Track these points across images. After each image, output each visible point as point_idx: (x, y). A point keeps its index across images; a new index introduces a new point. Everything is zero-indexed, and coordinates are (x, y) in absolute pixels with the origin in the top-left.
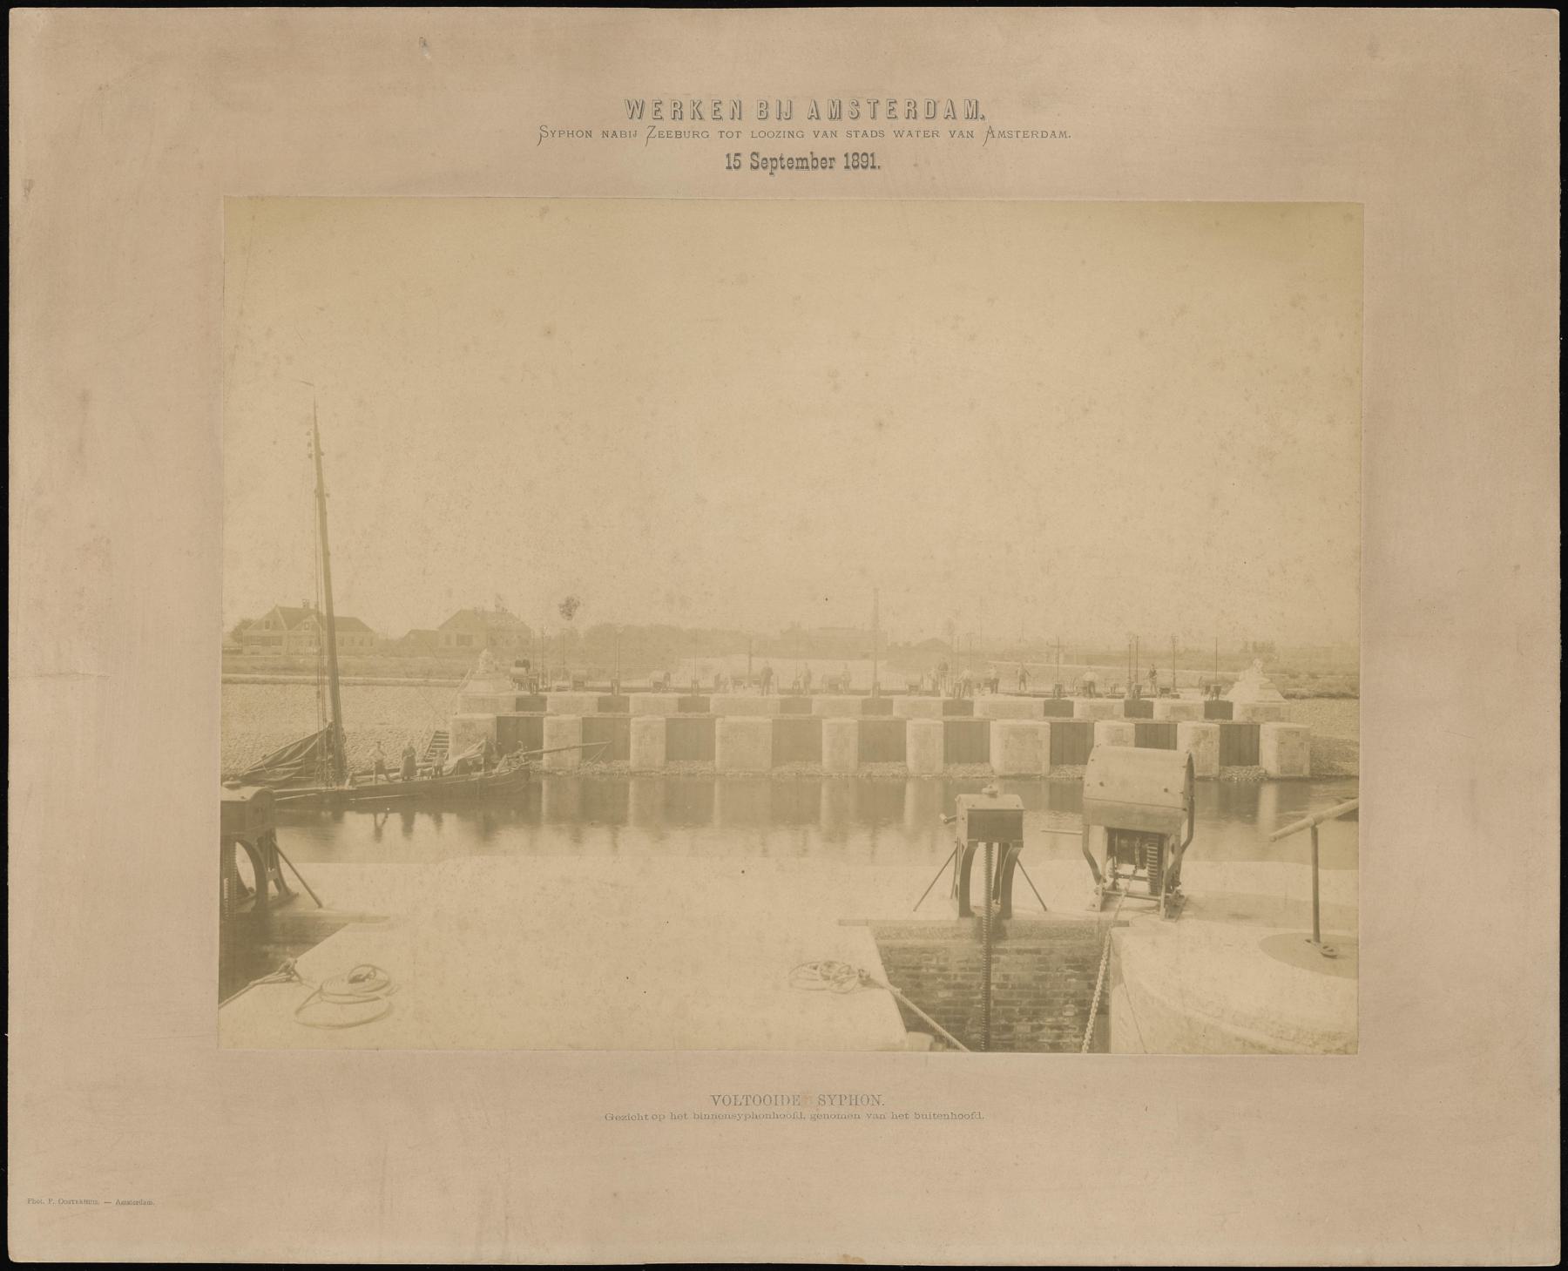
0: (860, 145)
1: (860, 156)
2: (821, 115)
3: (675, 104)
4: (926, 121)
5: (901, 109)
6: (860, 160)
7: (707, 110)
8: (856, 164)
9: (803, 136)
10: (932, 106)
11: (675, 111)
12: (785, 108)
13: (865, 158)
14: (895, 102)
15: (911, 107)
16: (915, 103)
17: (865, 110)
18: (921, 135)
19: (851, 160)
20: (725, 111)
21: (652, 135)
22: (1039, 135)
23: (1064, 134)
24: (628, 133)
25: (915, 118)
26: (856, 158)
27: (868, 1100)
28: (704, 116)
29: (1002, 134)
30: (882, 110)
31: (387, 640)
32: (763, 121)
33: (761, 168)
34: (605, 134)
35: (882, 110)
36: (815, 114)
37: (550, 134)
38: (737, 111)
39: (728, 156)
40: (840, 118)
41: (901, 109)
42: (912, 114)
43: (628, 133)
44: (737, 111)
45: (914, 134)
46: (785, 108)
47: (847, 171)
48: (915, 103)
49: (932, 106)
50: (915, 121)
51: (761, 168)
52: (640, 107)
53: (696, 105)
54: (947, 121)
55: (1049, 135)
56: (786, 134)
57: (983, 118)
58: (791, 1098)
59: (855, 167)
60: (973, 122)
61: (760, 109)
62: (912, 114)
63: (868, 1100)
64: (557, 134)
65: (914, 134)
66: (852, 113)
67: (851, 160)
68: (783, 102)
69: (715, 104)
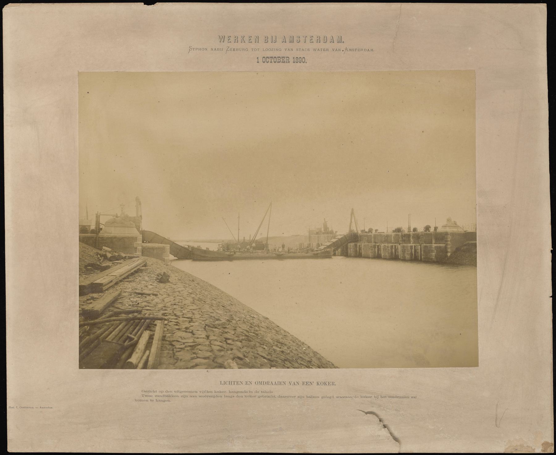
0: (300, 54)
1: (302, 58)
2: (286, 41)
3: (235, 37)
4: (310, 43)
5: (315, 39)
6: (299, 60)
7: (246, 39)
8: (297, 61)
9: (281, 50)
10: (325, 38)
11: (235, 40)
12: (274, 39)
13: (300, 59)
14: (313, 37)
15: (236, 38)
16: (320, 37)
17: (302, 39)
18: (322, 50)
19: (295, 60)
20: (253, 40)
21: (228, 50)
22: (364, 50)
23: (372, 50)
24: (220, 49)
25: (237, 42)
26: (297, 59)
27: (321, 383)
28: (246, 42)
29: (350, 50)
30: (308, 40)
31: (345, 236)
32: (266, 43)
33: (299, 62)
34: (292, 50)
35: (308, 40)
36: (332, 40)
37: (193, 49)
38: (257, 40)
39: (294, 58)
40: (293, 42)
41: (315, 39)
42: (236, 41)
43: (220, 49)
44: (257, 40)
45: (320, 50)
46: (274, 39)
47: (294, 63)
48: (320, 37)
49: (325, 38)
50: (319, 43)
51: (299, 62)
52: (257, 37)
53: (243, 37)
54: (283, 43)
55: (367, 50)
56: (275, 50)
57: (343, 42)
58: (324, 383)
59: (297, 62)
60: (340, 44)
61: (235, 39)
62: (236, 41)
63: (321, 383)
64: (195, 49)
65: (320, 50)
66: (297, 41)
67: (295, 60)
68: (273, 36)
69: (311, 37)
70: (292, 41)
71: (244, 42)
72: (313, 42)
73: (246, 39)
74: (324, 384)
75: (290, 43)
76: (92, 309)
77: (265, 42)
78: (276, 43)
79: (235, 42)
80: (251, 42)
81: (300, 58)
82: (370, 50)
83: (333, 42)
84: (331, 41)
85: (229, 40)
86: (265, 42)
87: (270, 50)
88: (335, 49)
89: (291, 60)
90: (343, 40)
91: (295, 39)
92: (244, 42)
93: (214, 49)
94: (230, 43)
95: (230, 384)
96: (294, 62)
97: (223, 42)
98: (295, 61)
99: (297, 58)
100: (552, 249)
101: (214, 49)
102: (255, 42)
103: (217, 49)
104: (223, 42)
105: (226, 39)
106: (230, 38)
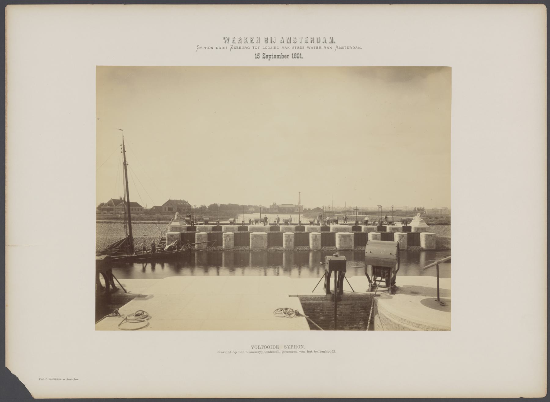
0: (297, 51)
3: (312, 38)
5: (309, 40)
7: (249, 40)
10: (319, 39)
12: (273, 40)
13: (298, 55)
18: (316, 48)
22: (352, 48)
29: (340, 48)
30: (303, 40)
35: (303, 40)
36: (283, 41)
39: (256, 54)
40: (290, 43)
41: (309, 40)
42: (240, 42)
43: (224, 48)
45: (313, 48)
47: (293, 59)
49: (319, 39)
53: (246, 38)
54: (281, 44)
56: (274, 48)
57: (335, 43)
60: (332, 44)
62: (240, 42)
64: (202, 48)
70: (289, 42)
71: (247, 43)
72: (308, 42)
73: (249, 40)
74: (276, 348)
75: (330, 44)
76: (370, 286)
77: (265, 43)
78: (275, 44)
79: (239, 43)
80: (308, 42)
81: (298, 54)
82: (358, 47)
83: (283, 43)
84: (281, 41)
85: (234, 41)
86: (265, 43)
87: (269, 48)
88: (327, 47)
89: (291, 56)
90: (334, 41)
91: (292, 40)
92: (247, 43)
93: (219, 48)
94: (307, 44)
95: (295, 347)
96: (293, 58)
97: (228, 43)
98: (294, 57)
99: (295, 54)
100: (207, 208)
101: (219, 48)
102: (257, 43)
103: (221, 48)
104: (228, 43)
105: (231, 40)
106: (234, 39)
